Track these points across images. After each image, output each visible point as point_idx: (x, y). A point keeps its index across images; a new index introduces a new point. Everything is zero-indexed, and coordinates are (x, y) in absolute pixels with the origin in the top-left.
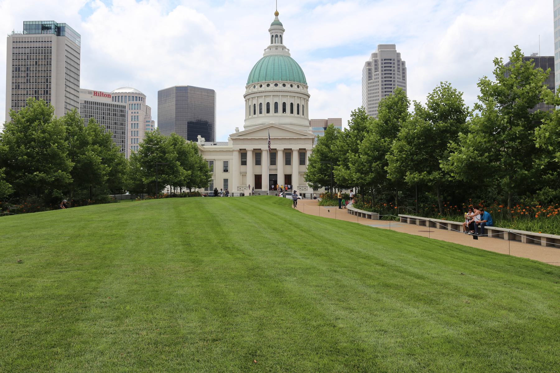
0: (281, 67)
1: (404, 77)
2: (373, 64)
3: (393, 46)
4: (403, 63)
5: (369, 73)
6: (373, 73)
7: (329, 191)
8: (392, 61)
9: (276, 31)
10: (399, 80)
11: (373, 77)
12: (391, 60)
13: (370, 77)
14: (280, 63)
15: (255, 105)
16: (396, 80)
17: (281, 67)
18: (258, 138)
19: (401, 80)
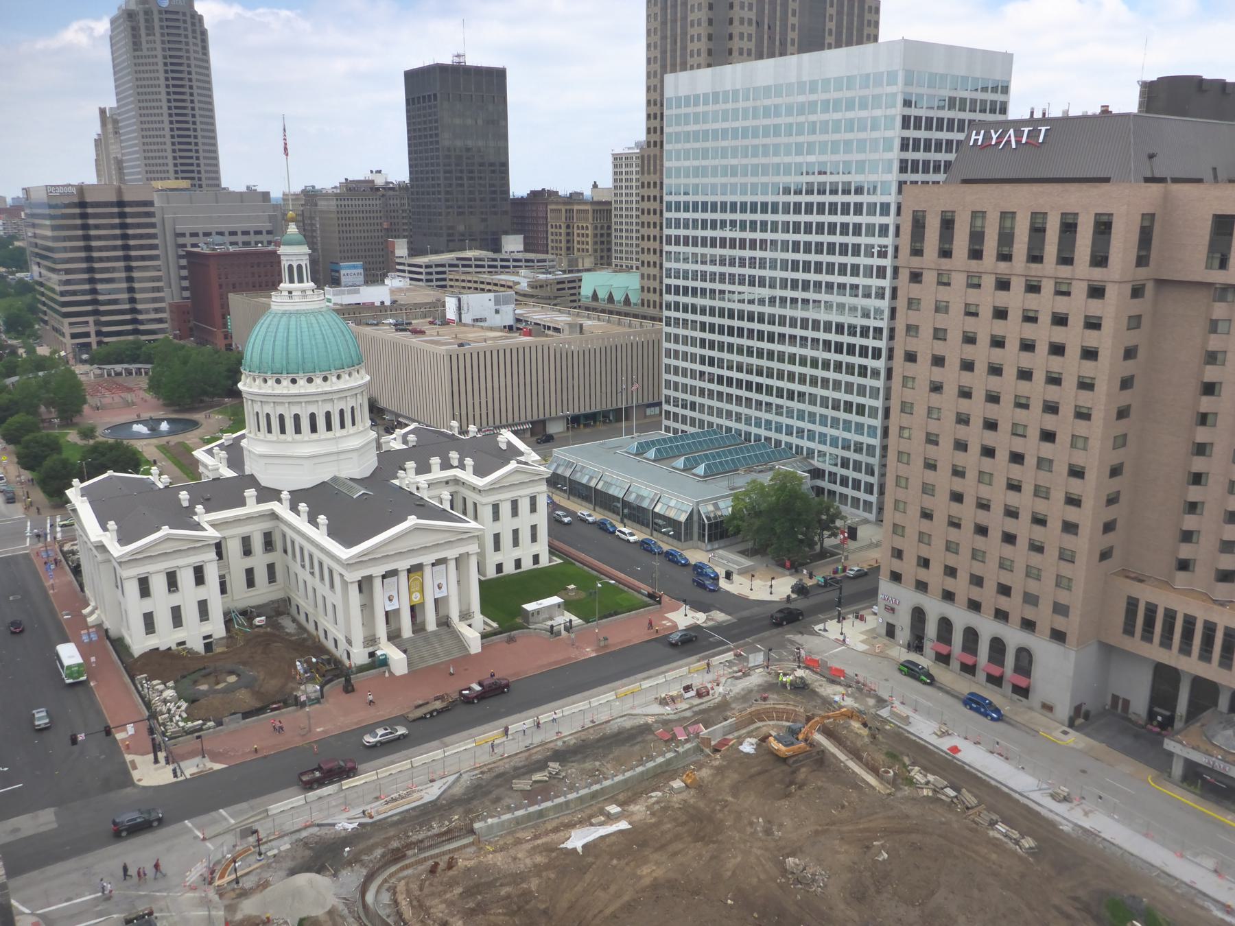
0: (302, 345)
1: (205, 49)
2: (141, 18)
3: (617, 158)
4: (201, 18)
5: (134, 36)
6: (144, 38)
7: (688, 746)
8: (180, 17)
9: (299, 258)
10: (196, 55)
11: (145, 46)
12: (177, 13)
13: (136, 45)
14: (315, 351)
15: (257, 413)
16: (192, 55)
17: (302, 345)
18: (380, 556)
19: (200, 56)
